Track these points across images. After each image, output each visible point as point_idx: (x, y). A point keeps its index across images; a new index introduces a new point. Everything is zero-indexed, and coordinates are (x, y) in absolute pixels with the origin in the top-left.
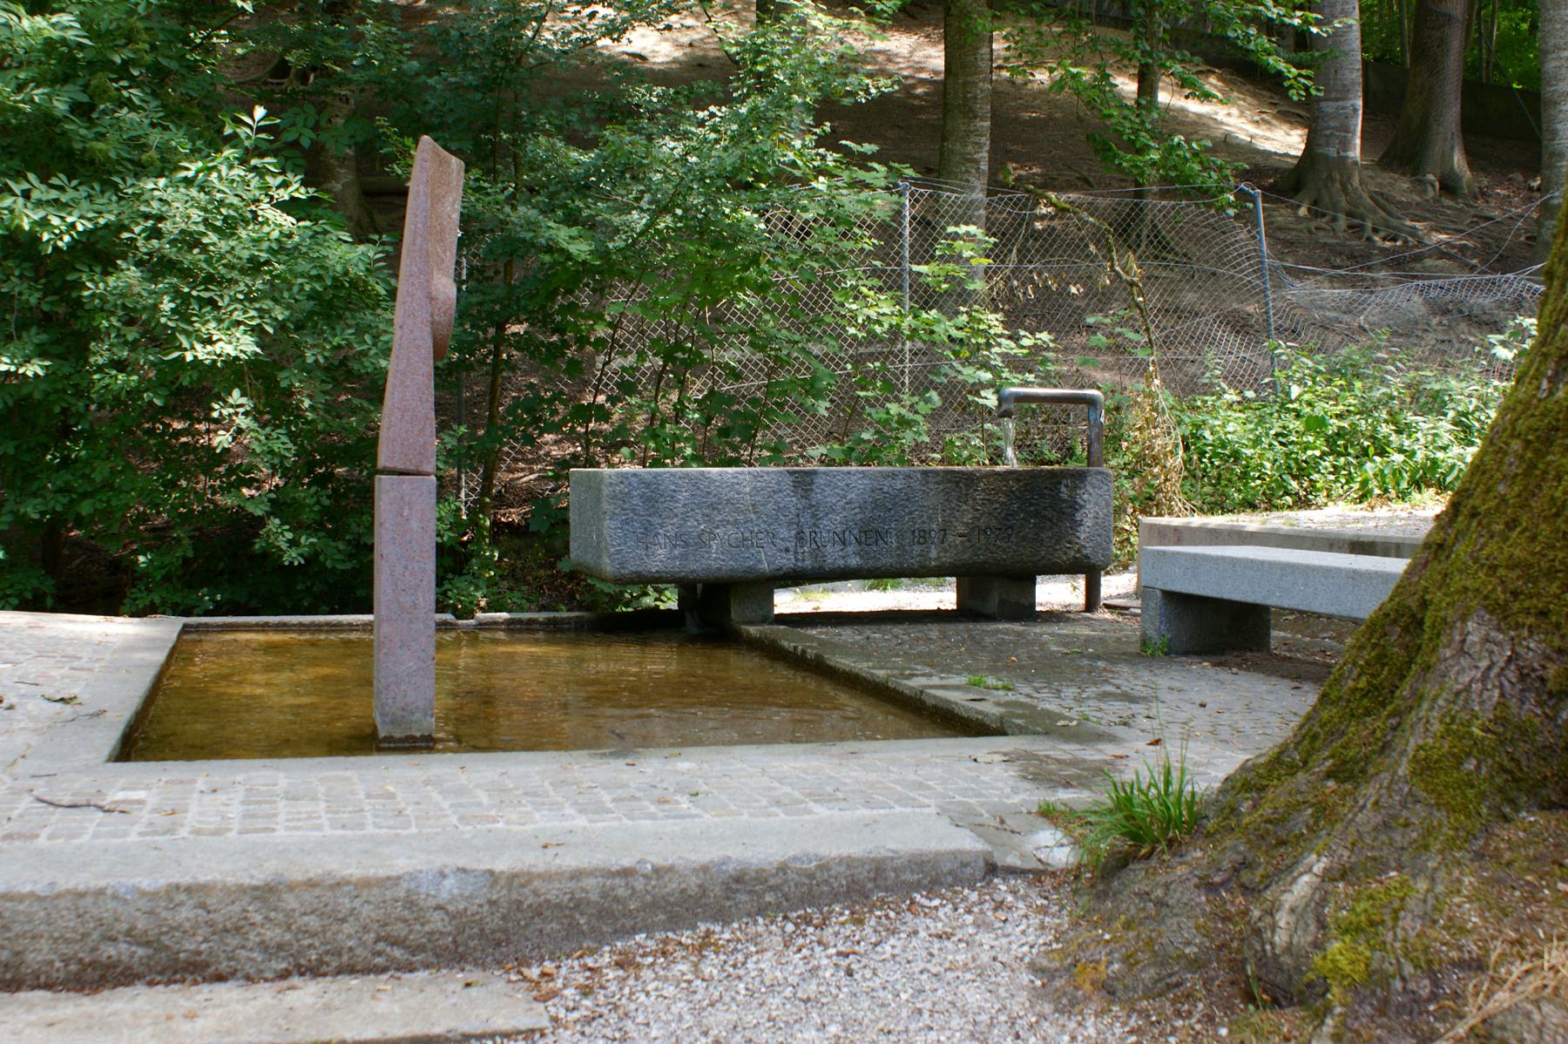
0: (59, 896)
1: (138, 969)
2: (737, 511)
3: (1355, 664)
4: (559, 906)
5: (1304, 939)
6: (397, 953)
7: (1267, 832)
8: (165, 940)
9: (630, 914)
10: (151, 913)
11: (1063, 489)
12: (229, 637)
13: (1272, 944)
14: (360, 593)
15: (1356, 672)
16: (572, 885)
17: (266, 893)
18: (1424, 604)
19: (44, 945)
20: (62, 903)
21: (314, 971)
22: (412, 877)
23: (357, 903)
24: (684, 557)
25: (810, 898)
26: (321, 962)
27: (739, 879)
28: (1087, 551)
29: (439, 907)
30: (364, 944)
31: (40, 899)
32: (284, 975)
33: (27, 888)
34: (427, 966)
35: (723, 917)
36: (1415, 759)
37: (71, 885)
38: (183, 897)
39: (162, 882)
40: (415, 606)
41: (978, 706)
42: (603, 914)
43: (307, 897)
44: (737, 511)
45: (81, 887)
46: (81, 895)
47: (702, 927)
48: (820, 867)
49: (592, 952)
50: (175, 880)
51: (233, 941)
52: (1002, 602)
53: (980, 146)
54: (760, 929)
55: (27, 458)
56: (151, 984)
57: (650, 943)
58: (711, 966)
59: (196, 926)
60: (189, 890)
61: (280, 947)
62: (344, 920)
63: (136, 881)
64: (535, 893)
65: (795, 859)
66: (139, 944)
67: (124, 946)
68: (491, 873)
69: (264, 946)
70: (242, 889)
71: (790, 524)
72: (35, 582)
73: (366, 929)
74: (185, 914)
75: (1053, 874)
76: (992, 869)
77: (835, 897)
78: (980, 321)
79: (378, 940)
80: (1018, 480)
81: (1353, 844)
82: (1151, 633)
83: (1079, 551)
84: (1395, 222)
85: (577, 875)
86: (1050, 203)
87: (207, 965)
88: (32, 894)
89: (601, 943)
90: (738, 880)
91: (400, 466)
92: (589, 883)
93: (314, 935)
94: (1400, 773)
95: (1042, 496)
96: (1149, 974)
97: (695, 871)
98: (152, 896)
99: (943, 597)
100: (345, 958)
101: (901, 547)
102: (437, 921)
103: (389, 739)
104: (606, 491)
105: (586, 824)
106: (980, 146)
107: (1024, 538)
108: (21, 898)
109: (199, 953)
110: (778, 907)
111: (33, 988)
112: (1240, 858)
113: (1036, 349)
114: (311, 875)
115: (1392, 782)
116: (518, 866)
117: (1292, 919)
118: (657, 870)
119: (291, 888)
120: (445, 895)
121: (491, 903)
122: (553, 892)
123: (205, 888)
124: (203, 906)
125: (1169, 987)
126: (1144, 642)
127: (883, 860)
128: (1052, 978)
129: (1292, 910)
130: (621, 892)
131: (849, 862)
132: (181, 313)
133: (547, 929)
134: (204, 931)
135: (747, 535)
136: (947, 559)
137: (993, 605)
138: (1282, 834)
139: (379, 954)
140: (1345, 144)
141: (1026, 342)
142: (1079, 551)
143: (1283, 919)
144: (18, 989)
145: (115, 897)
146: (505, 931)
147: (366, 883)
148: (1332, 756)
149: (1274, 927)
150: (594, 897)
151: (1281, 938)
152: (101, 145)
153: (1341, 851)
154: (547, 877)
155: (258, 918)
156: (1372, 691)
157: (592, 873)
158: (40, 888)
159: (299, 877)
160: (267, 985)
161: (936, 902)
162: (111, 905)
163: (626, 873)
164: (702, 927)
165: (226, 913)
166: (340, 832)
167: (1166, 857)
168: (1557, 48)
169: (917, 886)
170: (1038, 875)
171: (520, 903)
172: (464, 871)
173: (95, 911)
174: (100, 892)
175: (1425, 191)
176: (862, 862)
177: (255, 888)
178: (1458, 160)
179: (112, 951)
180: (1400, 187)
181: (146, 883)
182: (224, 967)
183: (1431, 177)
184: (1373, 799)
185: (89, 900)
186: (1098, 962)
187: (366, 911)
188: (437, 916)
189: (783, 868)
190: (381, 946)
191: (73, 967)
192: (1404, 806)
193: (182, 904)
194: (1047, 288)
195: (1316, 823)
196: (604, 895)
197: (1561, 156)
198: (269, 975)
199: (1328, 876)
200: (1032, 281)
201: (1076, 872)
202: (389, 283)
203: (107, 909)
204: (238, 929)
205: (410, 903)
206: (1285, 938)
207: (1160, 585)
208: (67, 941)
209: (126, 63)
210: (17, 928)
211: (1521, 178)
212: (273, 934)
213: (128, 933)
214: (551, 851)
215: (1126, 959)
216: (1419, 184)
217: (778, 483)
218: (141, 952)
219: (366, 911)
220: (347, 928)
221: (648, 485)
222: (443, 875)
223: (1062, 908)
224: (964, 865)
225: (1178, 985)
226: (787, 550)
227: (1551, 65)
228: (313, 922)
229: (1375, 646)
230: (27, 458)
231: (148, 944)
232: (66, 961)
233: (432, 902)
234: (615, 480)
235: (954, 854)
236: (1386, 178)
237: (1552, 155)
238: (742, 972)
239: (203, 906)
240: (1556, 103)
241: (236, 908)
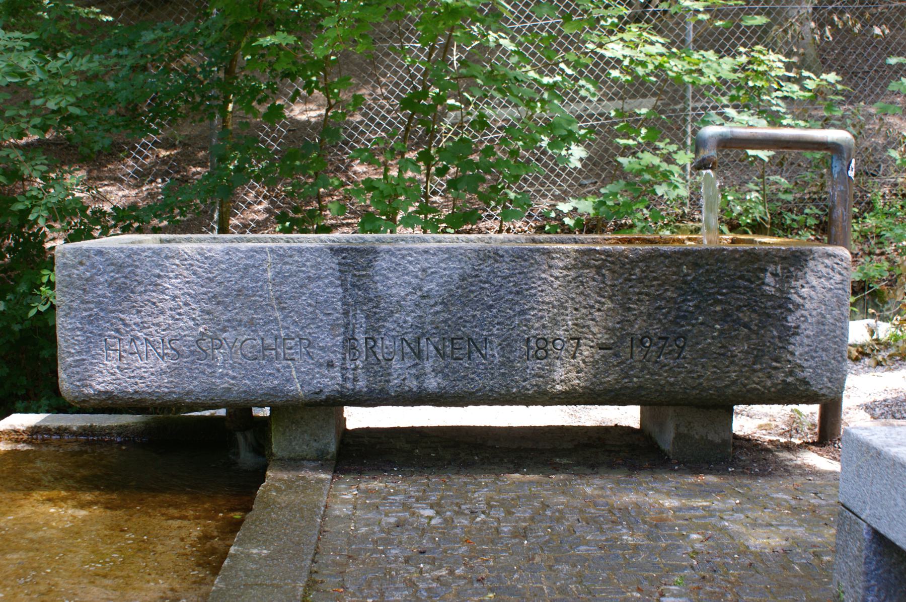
11: (769, 279)
14: (45, 354)
24: (175, 371)
28: (807, 374)
52: (679, 436)
71: (334, 326)
78: (761, 62)
80: (696, 265)
83: (791, 373)
95: (733, 288)
101: (507, 363)
107: (704, 353)
113: (818, 93)
135: (269, 341)
136: (577, 382)
141: (810, 84)
142: (791, 373)
194: (849, 30)
200: (832, 24)
202: (510, 55)
217: (317, 266)
221: (120, 267)
226: (330, 365)
234: (71, 260)
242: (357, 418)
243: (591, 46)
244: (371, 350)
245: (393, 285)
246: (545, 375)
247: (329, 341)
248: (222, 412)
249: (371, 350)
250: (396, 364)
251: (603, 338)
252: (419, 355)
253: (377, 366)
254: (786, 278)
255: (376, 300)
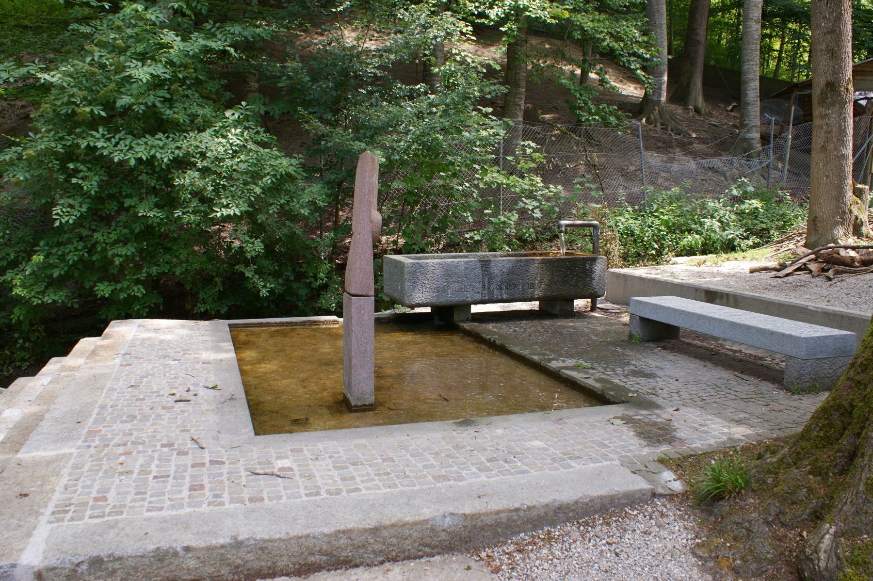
0: (291, 539)
1: (323, 565)
2: (459, 277)
3: (817, 425)
4: (491, 525)
5: (832, 565)
6: (427, 549)
7: (787, 497)
8: (334, 553)
9: (518, 526)
10: (329, 542)
12: (251, 329)
13: (819, 567)
15: (818, 429)
16: (496, 516)
17: (375, 531)
18: (852, 406)
19: (285, 559)
20: (292, 541)
21: (395, 560)
22: (433, 519)
23: (411, 532)
24: (437, 296)
25: (586, 513)
26: (397, 556)
27: (560, 508)
29: (444, 530)
30: (414, 547)
31: (283, 540)
32: (382, 563)
33: (278, 536)
34: (439, 554)
35: (553, 524)
36: (866, 484)
37: (295, 534)
38: (342, 535)
39: (333, 529)
40: (366, 351)
41: (586, 381)
42: (508, 527)
43: (392, 531)
44: (459, 277)
45: (300, 534)
46: (300, 538)
47: (546, 529)
48: (590, 501)
49: (505, 543)
50: (338, 528)
51: (362, 551)
52: (561, 310)
53: (521, 99)
54: (569, 528)
55: (151, 249)
56: (329, 570)
57: (527, 538)
58: (557, 549)
59: (347, 546)
60: (344, 532)
61: (381, 551)
62: (406, 539)
63: (322, 529)
64: (482, 521)
65: (581, 498)
66: (324, 555)
67: (317, 557)
68: (465, 514)
69: (374, 552)
70: (365, 530)
72: (155, 300)
73: (415, 541)
74: (343, 541)
75: (677, 495)
76: (654, 495)
77: (596, 512)
79: (420, 545)
81: (845, 520)
82: (634, 332)
84: (680, 127)
85: (498, 512)
86: (558, 129)
87: (351, 561)
88: (280, 539)
89: (507, 538)
90: (559, 508)
91: (359, 293)
92: (502, 515)
93: (395, 545)
94: (861, 489)
96: (754, 566)
97: (543, 507)
98: (329, 536)
99: (534, 305)
100: (406, 553)
102: (443, 536)
103: (356, 406)
104: (406, 270)
105: (485, 479)
106: (521, 99)
108: (276, 541)
109: (348, 557)
110: (574, 518)
111: (280, 576)
112: (778, 510)
114: (393, 522)
115: (857, 492)
116: (475, 511)
117: (826, 555)
118: (528, 508)
119: (385, 528)
120: (446, 525)
121: (464, 526)
122: (489, 520)
123: (350, 531)
124: (350, 538)
125: (763, 572)
126: (631, 336)
127: (614, 496)
128: (706, 561)
129: (825, 552)
130: (515, 518)
131: (601, 498)
132: (216, 191)
133: (486, 534)
134: (350, 548)
137: (557, 310)
138: (794, 499)
139: (420, 551)
140: (660, 95)
143: (822, 556)
144: (274, 577)
145: (314, 537)
146: (470, 537)
147: (415, 523)
148: (810, 464)
149: (819, 559)
150: (504, 520)
151: (822, 564)
152: (176, 116)
153: (840, 524)
154: (486, 514)
155: (372, 541)
156: (827, 438)
157: (503, 511)
158: (283, 536)
159: (388, 523)
160: (377, 568)
161: (635, 512)
162: (313, 540)
163: (517, 510)
164: (546, 529)
165: (359, 540)
166: (389, 490)
167: (737, 500)
168: (748, 60)
169: (626, 505)
170: (671, 496)
171: (475, 526)
172: (453, 514)
173: (306, 544)
174: (308, 536)
175: (689, 113)
176: (606, 497)
177: (371, 529)
178: (700, 99)
179: (313, 559)
180: (679, 110)
181: (326, 530)
182: (358, 561)
183: (691, 107)
184: (849, 500)
185: (303, 539)
186: (728, 558)
187: (415, 534)
188: (443, 534)
189: (576, 502)
190: (421, 547)
191: (297, 566)
192: (864, 503)
193: (341, 538)
195: (809, 495)
196: (508, 519)
197: (748, 104)
198: (376, 563)
199: (836, 535)
200: (551, 162)
201: (684, 496)
203: (310, 543)
204: (364, 546)
205: (432, 530)
206: (824, 564)
207: (638, 314)
208: (294, 556)
209: (185, 78)
210: (274, 553)
211: (723, 106)
212: (377, 547)
213: (319, 551)
214: (484, 500)
215: (742, 559)
216: (686, 109)
218: (324, 558)
219: (415, 534)
220: (407, 542)
222: (445, 517)
223: (690, 516)
224: (644, 495)
225: (766, 571)
227: (745, 67)
228: (394, 541)
229: (826, 419)
230: (151, 249)
231: (327, 555)
232: (294, 564)
233: (441, 528)
235: (640, 491)
236: (673, 107)
237: (745, 103)
238: (571, 554)
239: (350, 538)
240: (747, 83)
241: (363, 537)
242: (475, 309)
243: (777, 46)
244: (489, 288)
245: (495, 270)
246: (533, 293)
247: (479, 286)
248: (428, 310)
249: (489, 288)
250: (495, 292)
251: (547, 282)
252: (501, 289)
253: (491, 292)
254: (591, 265)
255: (490, 274)
